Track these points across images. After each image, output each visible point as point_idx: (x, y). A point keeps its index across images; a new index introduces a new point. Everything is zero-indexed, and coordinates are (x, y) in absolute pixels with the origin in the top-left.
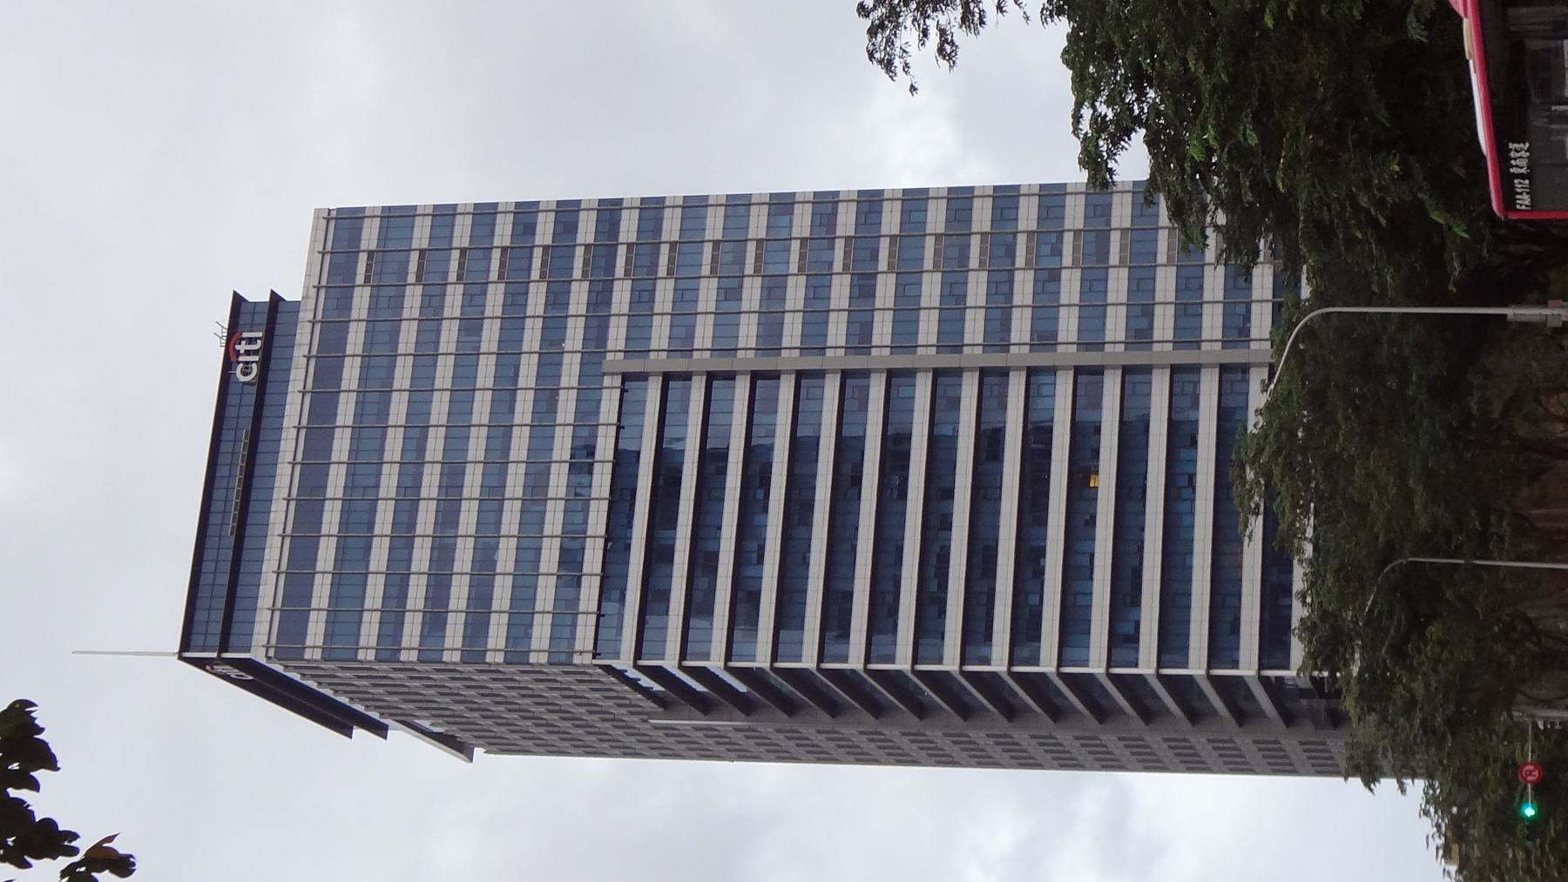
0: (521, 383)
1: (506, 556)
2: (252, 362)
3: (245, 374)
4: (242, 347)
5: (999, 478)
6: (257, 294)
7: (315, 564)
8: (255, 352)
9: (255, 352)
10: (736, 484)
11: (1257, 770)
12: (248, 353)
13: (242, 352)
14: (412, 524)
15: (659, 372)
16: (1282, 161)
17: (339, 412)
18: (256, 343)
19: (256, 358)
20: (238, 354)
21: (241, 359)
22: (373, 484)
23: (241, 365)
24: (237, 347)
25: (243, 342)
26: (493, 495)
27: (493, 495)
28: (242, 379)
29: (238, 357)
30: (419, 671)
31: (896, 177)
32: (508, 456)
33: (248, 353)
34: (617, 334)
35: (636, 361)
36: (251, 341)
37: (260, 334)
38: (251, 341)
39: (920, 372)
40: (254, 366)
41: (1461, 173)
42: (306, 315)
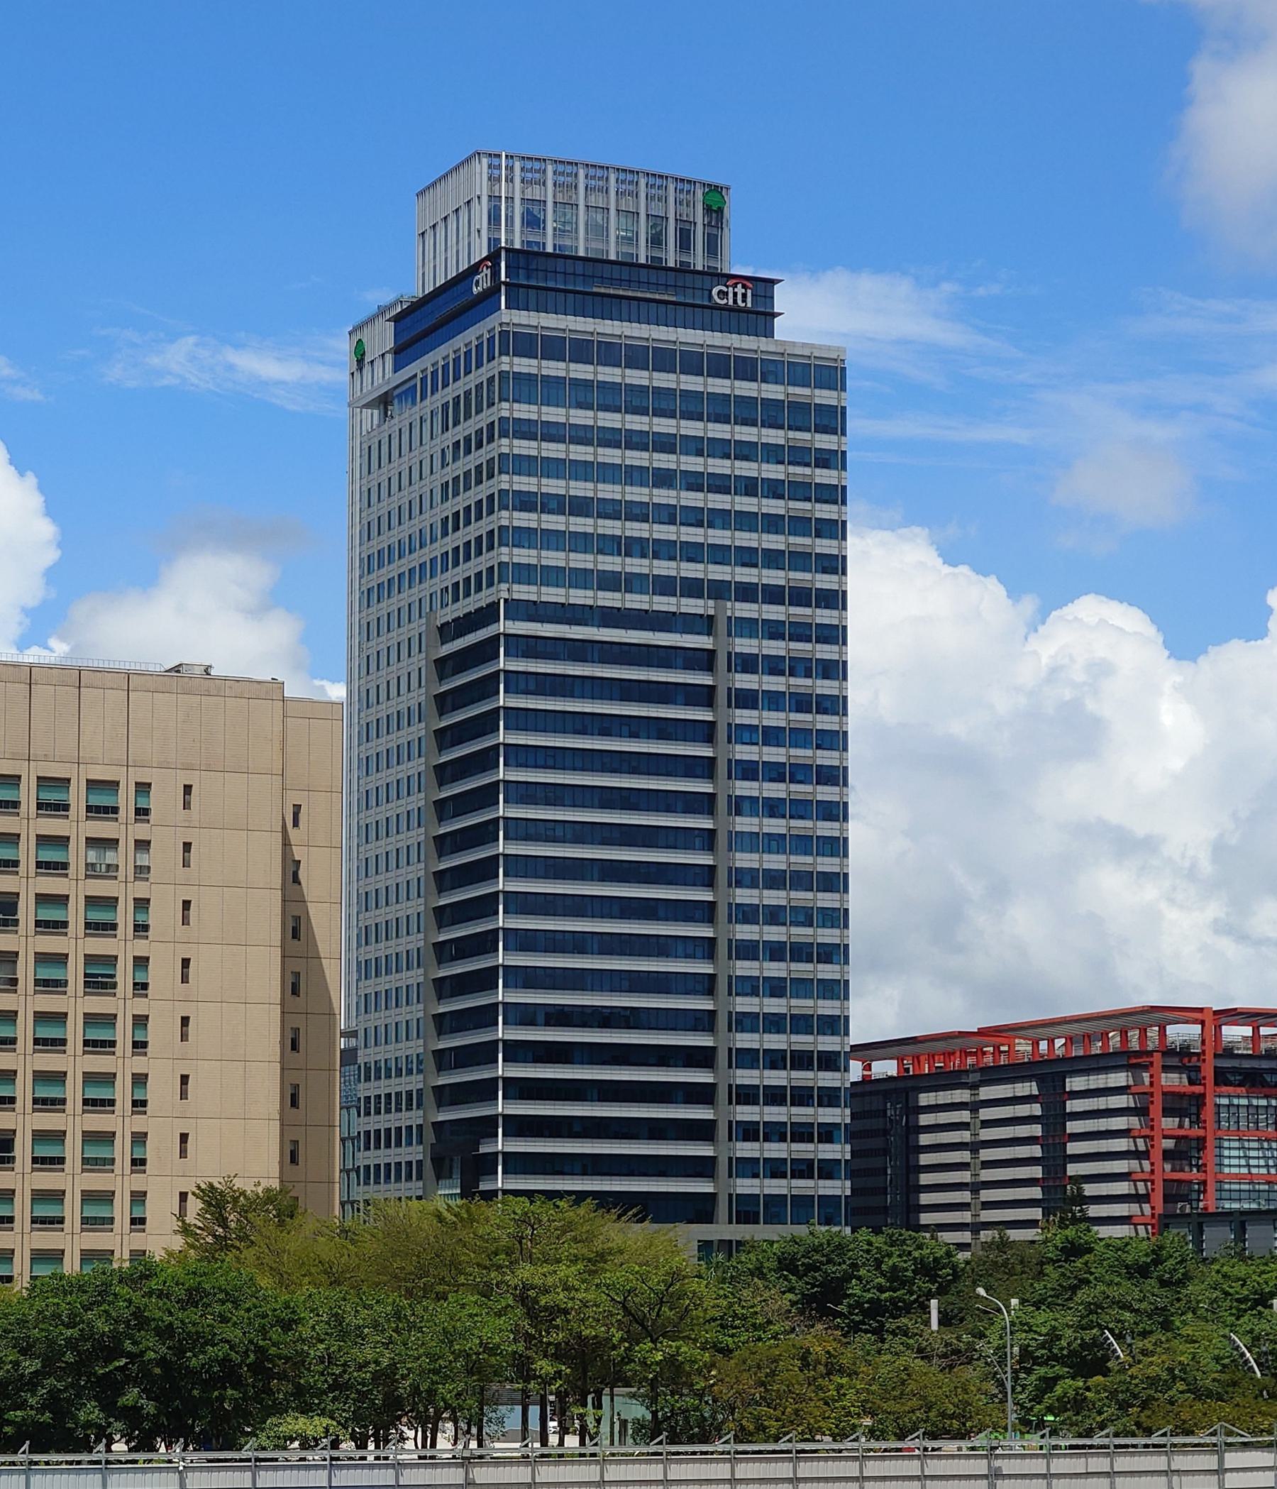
1: (554, 486)
3: (720, 292)
4: (740, 290)
5: (651, 974)
8: (735, 301)
9: (735, 301)
11: (671, 1063)
12: (735, 294)
16: (889, 1172)
17: (638, 536)
19: (731, 302)
20: (735, 286)
21: (731, 289)
22: (538, 763)
24: (739, 286)
25: (743, 291)
28: (715, 291)
31: (857, 832)
33: (735, 294)
34: (746, 610)
36: (744, 296)
37: (459, 1191)
38: (744, 296)
41: (713, 1373)
42: (762, 344)
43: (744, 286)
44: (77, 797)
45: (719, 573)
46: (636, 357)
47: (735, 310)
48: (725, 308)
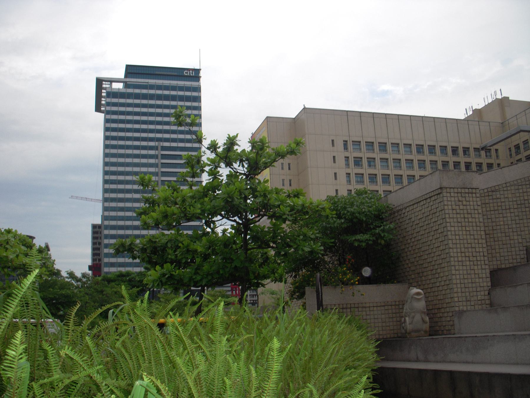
4: (191, 72)
12: (190, 73)
20: (190, 71)
33: (190, 73)
36: (192, 73)
38: (192, 73)
44: (461, 151)
45: (159, 135)
46: (159, 87)
47: (190, 76)
48: (187, 76)
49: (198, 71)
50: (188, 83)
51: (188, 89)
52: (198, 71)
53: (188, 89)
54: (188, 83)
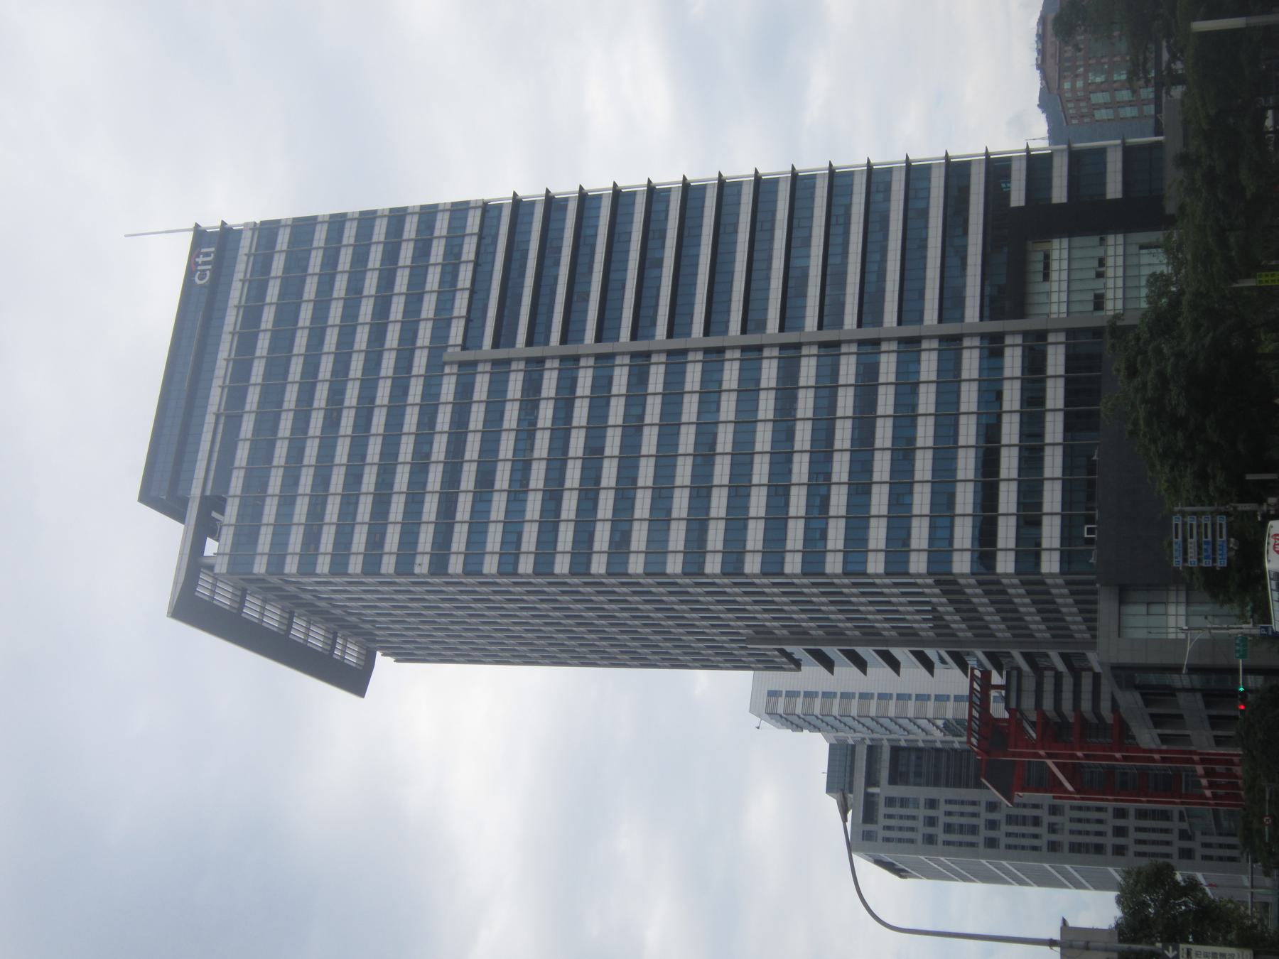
0: (524, 548)
2: (207, 270)
3: (201, 278)
4: (200, 260)
6: (211, 223)
7: (402, 427)
10: (702, 310)
12: (204, 263)
13: (200, 263)
14: (321, 516)
15: (1019, 331)
18: (210, 256)
19: (209, 267)
20: (197, 264)
23: (198, 273)
24: (197, 260)
25: (201, 256)
26: (779, 490)
27: (779, 490)
29: (197, 267)
30: (548, 651)
32: (832, 445)
33: (204, 263)
35: (795, 333)
36: (207, 255)
37: (213, 249)
38: (207, 255)
39: (965, 336)
40: (208, 273)
43: (198, 256)
49: (200, 236)
50: (241, 268)
51: (297, 261)
52: (200, 236)
53: (297, 261)
54: (241, 268)
